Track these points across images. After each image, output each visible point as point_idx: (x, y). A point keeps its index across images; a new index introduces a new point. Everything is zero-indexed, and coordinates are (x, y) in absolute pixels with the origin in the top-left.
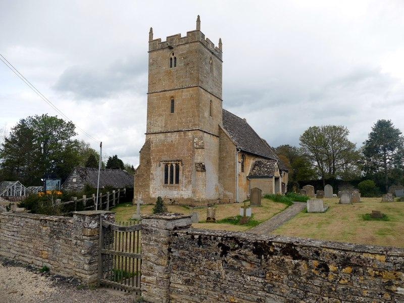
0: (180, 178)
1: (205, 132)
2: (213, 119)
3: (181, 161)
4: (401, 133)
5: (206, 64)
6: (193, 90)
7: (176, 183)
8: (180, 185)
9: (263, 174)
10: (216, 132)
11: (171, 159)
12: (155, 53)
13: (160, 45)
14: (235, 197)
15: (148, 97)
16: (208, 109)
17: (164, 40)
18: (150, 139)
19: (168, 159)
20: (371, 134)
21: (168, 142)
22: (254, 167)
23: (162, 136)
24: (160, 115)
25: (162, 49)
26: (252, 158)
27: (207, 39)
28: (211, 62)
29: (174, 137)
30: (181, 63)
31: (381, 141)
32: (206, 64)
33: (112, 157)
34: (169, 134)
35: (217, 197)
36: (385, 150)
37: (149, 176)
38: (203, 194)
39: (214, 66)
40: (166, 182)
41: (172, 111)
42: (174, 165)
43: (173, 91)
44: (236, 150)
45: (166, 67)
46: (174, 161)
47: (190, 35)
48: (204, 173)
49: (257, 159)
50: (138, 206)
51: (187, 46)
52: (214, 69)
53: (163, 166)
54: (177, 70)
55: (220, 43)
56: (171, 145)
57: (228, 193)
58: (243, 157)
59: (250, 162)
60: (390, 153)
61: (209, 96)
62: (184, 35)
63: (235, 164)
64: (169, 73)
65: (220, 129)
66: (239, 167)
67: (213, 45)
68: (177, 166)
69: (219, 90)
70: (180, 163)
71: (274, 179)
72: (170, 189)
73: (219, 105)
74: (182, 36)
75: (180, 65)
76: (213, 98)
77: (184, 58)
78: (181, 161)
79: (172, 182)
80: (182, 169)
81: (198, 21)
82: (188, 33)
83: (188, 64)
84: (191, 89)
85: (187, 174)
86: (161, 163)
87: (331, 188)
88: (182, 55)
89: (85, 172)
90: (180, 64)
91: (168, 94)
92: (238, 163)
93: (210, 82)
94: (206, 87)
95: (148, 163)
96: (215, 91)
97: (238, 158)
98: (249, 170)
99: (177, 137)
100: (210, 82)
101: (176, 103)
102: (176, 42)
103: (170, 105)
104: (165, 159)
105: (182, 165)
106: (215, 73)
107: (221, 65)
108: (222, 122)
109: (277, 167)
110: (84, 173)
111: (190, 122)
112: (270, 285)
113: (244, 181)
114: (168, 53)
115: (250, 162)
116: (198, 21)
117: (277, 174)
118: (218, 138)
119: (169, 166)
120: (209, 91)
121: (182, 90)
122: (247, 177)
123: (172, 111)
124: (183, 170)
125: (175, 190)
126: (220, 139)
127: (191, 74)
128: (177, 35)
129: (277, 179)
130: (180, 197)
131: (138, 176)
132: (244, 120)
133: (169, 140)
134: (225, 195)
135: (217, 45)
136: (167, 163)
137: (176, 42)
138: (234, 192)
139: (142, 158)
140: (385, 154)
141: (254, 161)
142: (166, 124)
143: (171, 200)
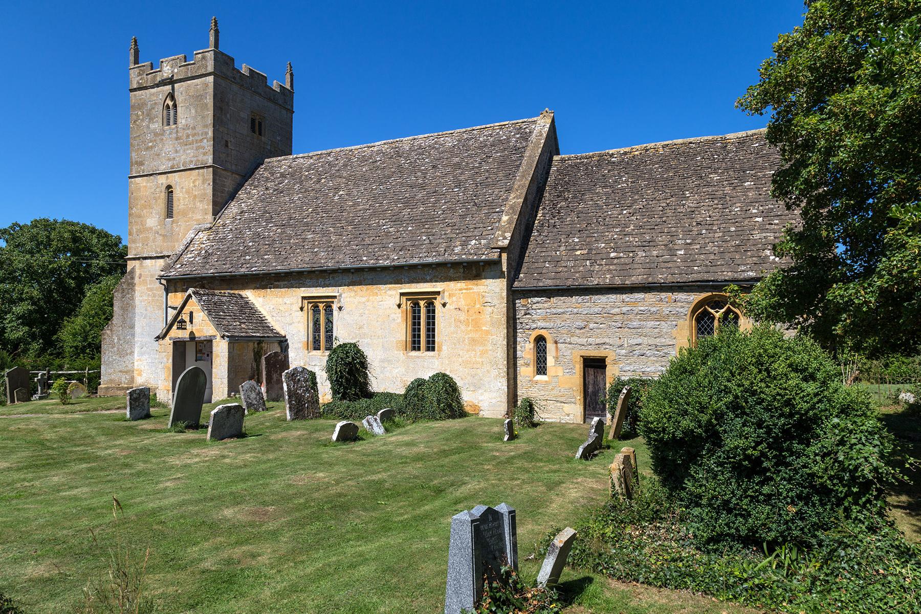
120: (162, 169)
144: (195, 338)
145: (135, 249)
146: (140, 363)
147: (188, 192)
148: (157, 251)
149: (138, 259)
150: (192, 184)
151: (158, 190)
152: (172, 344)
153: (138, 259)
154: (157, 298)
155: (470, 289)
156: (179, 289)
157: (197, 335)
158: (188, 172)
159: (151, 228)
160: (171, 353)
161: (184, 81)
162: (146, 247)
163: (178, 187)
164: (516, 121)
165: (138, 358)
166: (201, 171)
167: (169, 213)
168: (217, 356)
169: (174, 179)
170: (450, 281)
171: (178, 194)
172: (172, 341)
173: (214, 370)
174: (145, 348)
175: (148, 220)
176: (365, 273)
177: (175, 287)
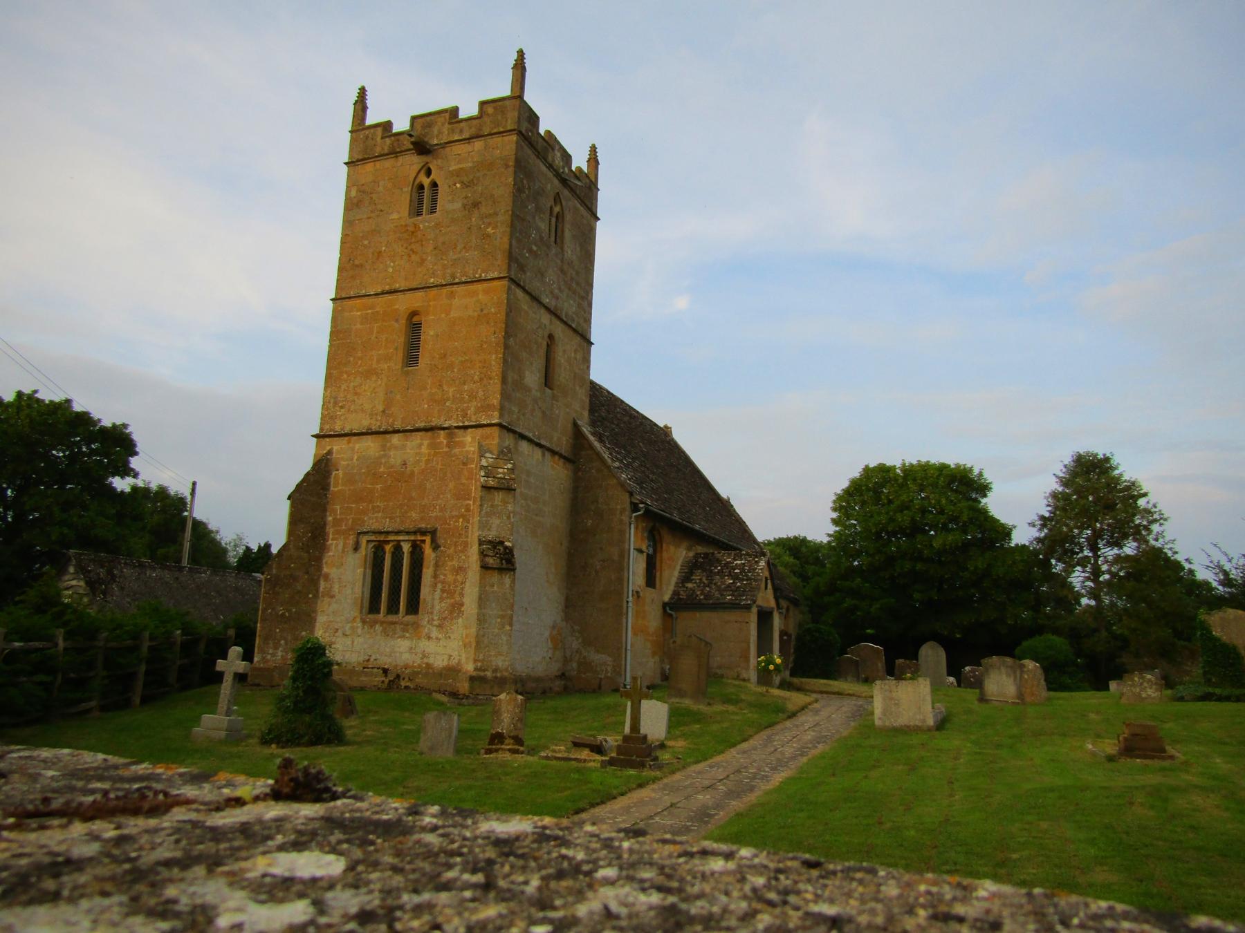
0: (425, 591)
1: (523, 437)
2: (554, 397)
3: (433, 533)
4: (1145, 495)
5: (538, 209)
6: (486, 292)
7: (408, 612)
8: (423, 618)
9: (717, 594)
10: (561, 441)
11: (396, 526)
12: (369, 167)
13: (388, 141)
14: (619, 669)
15: (335, 311)
16: (539, 363)
17: (401, 125)
18: (330, 452)
19: (387, 525)
20: (1054, 495)
21: (392, 467)
22: (691, 573)
23: (369, 446)
24: (369, 373)
25: (394, 153)
26: (685, 544)
27: (548, 132)
28: (557, 209)
29: (413, 450)
30: (452, 201)
31: (1087, 517)
32: (538, 209)
33: (255, 548)
34: (396, 439)
35: (555, 668)
36: (1094, 548)
37: (314, 582)
38: (500, 654)
39: (567, 227)
40: (374, 607)
41: (411, 356)
42: (406, 548)
43: (420, 294)
44: (628, 506)
45: (399, 213)
46: (408, 533)
47: (490, 110)
48: (507, 580)
49: (700, 549)
50: (227, 685)
51: (478, 145)
52: (567, 234)
53: (365, 549)
54: (438, 225)
55: (594, 160)
56: (401, 476)
57: (596, 657)
58: (654, 537)
59: (677, 556)
60: (1110, 552)
61: (545, 318)
62: (469, 110)
63: (624, 555)
64: (410, 235)
65: (577, 433)
66: (637, 568)
67: (567, 158)
68: (417, 549)
69: (579, 306)
70: (428, 539)
71: (753, 617)
72: (385, 633)
73: (579, 356)
74: (462, 115)
75: (450, 207)
76: (559, 330)
77: (465, 185)
78: (433, 533)
79: (393, 608)
80: (433, 562)
81: (520, 67)
82: (483, 104)
83: (476, 205)
84: (479, 286)
85: (450, 578)
86: (364, 540)
87: (942, 654)
88: (458, 173)
89: (110, 572)
90: (449, 203)
91: (404, 303)
92: (633, 553)
93: (552, 275)
94: (535, 285)
95: (314, 537)
96: (568, 307)
97: (635, 538)
98: (674, 580)
99: (424, 450)
100: (552, 275)
101: (429, 334)
102: (440, 132)
103: (401, 340)
104: (375, 526)
105: (436, 547)
106: (571, 250)
107: (592, 230)
108: (586, 414)
109: (767, 574)
110: (102, 572)
111: (473, 396)
112: (1041, 859)
113: (653, 620)
114: (411, 164)
115: (677, 556)
116: (520, 67)
117: (766, 598)
118: (569, 466)
119: (388, 548)
120: (546, 300)
121: (448, 289)
122: (665, 605)
123: (411, 356)
124: (437, 565)
125: (403, 637)
126: (576, 471)
127: (486, 236)
128: (445, 111)
129: (764, 617)
130: (419, 662)
131: (274, 583)
132: (666, 432)
133: (395, 458)
134: (585, 665)
135: (580, 161)
136: (382, 538)
137: (440, 132)
138: (617, 651)
139: (294, 520)
140: (1097, 557)
141: (691, 554)
142: (389, 404)
143: (385, 671)
150: (573, 355)
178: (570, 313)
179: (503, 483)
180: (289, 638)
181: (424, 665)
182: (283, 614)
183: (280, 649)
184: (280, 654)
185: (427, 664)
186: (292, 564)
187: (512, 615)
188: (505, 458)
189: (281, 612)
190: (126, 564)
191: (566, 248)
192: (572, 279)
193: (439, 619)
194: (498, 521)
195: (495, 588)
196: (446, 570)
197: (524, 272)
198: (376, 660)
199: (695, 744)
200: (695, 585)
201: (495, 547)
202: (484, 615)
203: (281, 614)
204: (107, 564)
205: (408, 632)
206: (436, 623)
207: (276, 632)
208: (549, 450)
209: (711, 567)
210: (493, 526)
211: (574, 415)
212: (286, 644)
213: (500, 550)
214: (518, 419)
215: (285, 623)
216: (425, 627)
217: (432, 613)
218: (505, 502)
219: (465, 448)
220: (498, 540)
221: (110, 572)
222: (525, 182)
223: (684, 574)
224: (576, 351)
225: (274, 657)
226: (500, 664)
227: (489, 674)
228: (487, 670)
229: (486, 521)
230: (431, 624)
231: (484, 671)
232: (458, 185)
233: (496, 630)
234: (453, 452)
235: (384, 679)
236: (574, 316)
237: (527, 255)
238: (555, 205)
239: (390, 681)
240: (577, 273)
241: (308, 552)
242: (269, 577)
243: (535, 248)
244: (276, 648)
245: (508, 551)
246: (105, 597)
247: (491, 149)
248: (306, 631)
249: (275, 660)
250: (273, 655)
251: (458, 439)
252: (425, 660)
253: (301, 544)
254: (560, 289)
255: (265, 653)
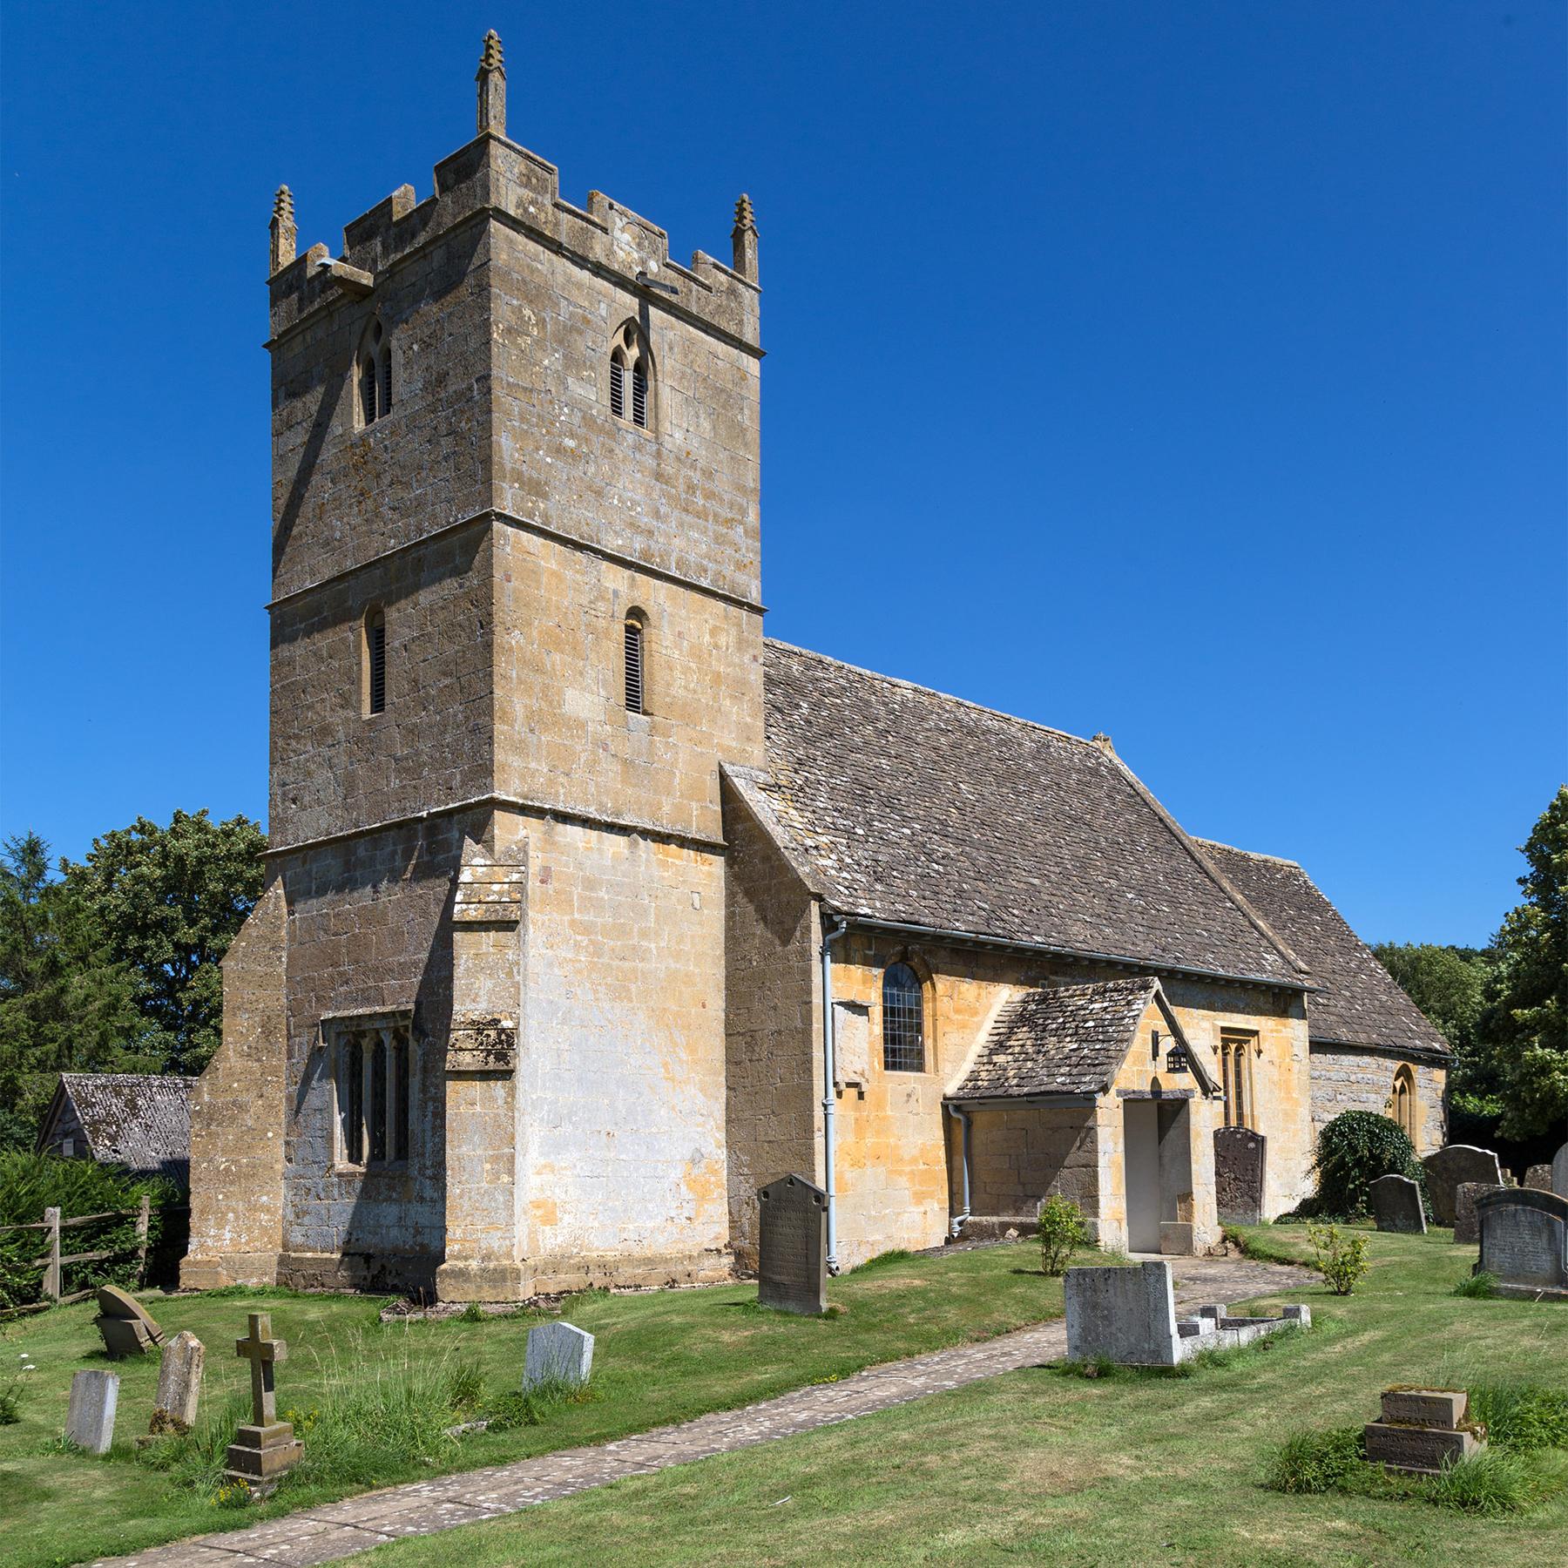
2: (653, 730)
5: (573, 362)
22: (1011, 1032)
61: (616, 578)
120: (612, 544)
125: (389, 1199)
144: (1161, 1092)
145: (522, 778)
146: (551, 1177)
147: (696, 653)
148: (601, 804)
149: (540, 813)
150: (707, 638)
151: (601, 606)
152: (1121, 1106)
153: (540, 813)
154: (606, 960)
155: (1281, 1031)
156: (858, 956)
157: (1164, 1088)
158: (697, 596)
159: (582, 725)
160: (1121, 1130)
161: (678, 317)
162: (562, 779)
163: (665, 623)
164: (1051, 729)
165: (542, 1161)
166: (733, 610)
167: (634, 699)
168: (1198, 1134)
169: (654, 595)
170: (1261, 1014)
171: (661, 643)
172: (1121, 1099)
173: (1194, 1167)
174: (567, 1128)
175: (570, 694)
176: (1174, 982)
177: (845, 947)
178: (692, 558)
179: (496, 911)
180: (241, 1208)
181: (418, 1248)
182: (227, 1170)
183: (228, 1228)
184: (228, 1236)
185: (422, 1245)
186: (234, 1082)
187: (513, 1156)
188: (510, 862)
189: (223, 1167)
190: (161, 1086)
191: (666, 427)
192: (691, 488)
193: (432, 1166)
194: (489, 984)
195: (478, 1108)
196: (436, 1077)
197: (545, 496)
198: (357, 1240)
199: (87, 1474)
200: (1010, 1058)
201: (480, 1032)
202: (459, 1159)
203: (224, 1169)
204: (126, 1091)
205: (395, 1191)
206: (429, 1172)
207: (218, 1200)
208: (646, 834)
209: (1046, 1019)
210: (481, 993)
211: (720, 756)
212: (237, 1218)
213: (488, 1036)
214: (552, 782)
215: (232, 1183)
216: (416, 1179)
217: (423, 1155)
218: (502, 947)
219: (451, 851)
220: (489, 1017)
221: (132, 1105)
222: (527, 312)
223: (996, 1038)
224: (714, 632)
225: (217, 1241)
226: (495, 1245)
227: (474, 1265)
228: (472, 1257)
229: (467, 985)
230: (424, 1175)
231: (466, 1258)
232: (415, 347)
233: (484, 1185)
234: (435, 861)
235: (366, 1273)
236: (705, 562)
237: (549, 460)
238: (628, 347)
239: (373, 1277)
240: (709, 474)
241: (259, 1060)
242: (198, 1108)
243: (570, 443)
244: (220, 1226)
245: (503, 1037)
246: (114, 1144)
247: (456, 261)
248: (267, 1194)
249: (221, 1246)
250: (218, 1238)
251: (441, 837)
252: (419, 1239)
253: (245, 1048)
254: (657, 514)
255: (203, 1237)
